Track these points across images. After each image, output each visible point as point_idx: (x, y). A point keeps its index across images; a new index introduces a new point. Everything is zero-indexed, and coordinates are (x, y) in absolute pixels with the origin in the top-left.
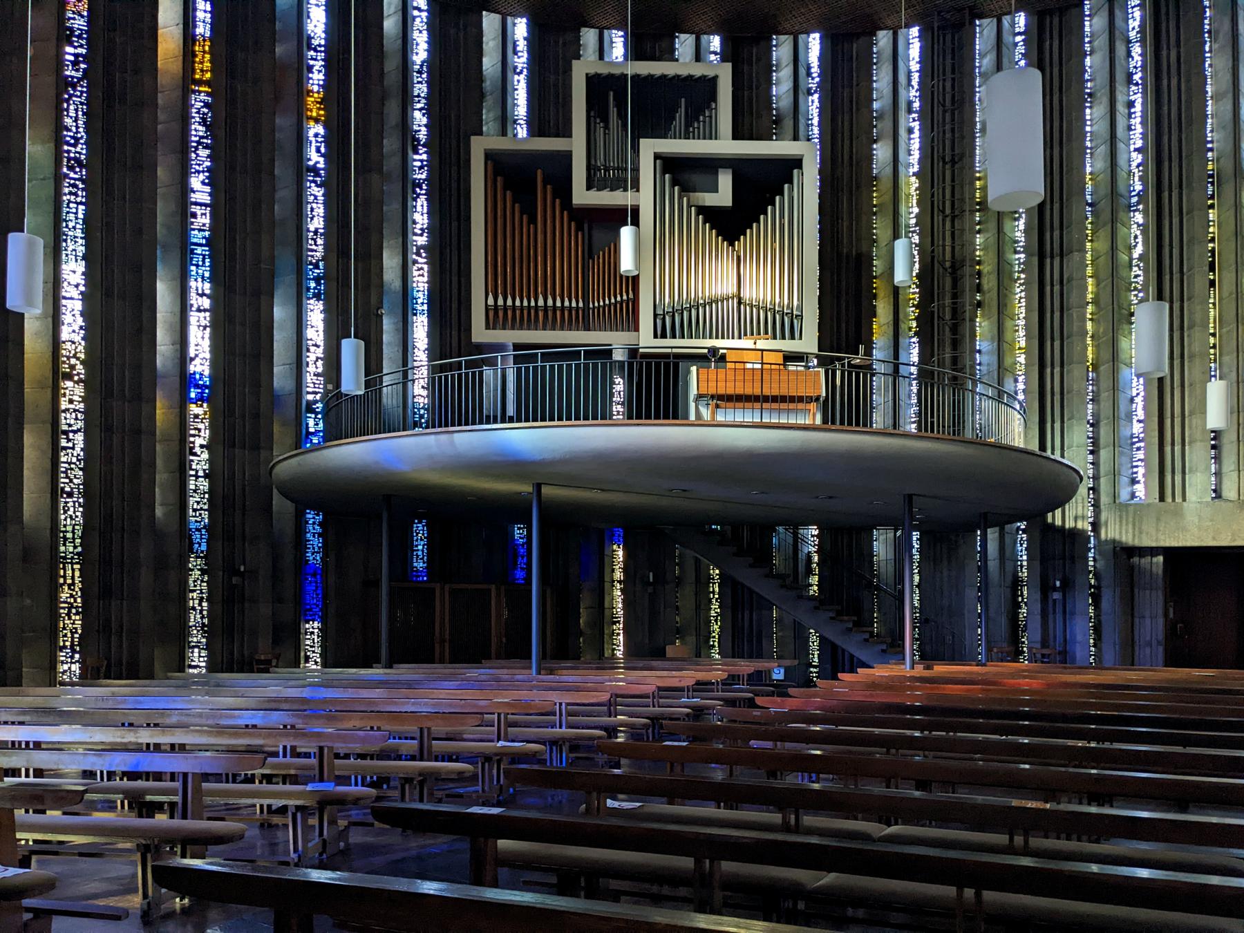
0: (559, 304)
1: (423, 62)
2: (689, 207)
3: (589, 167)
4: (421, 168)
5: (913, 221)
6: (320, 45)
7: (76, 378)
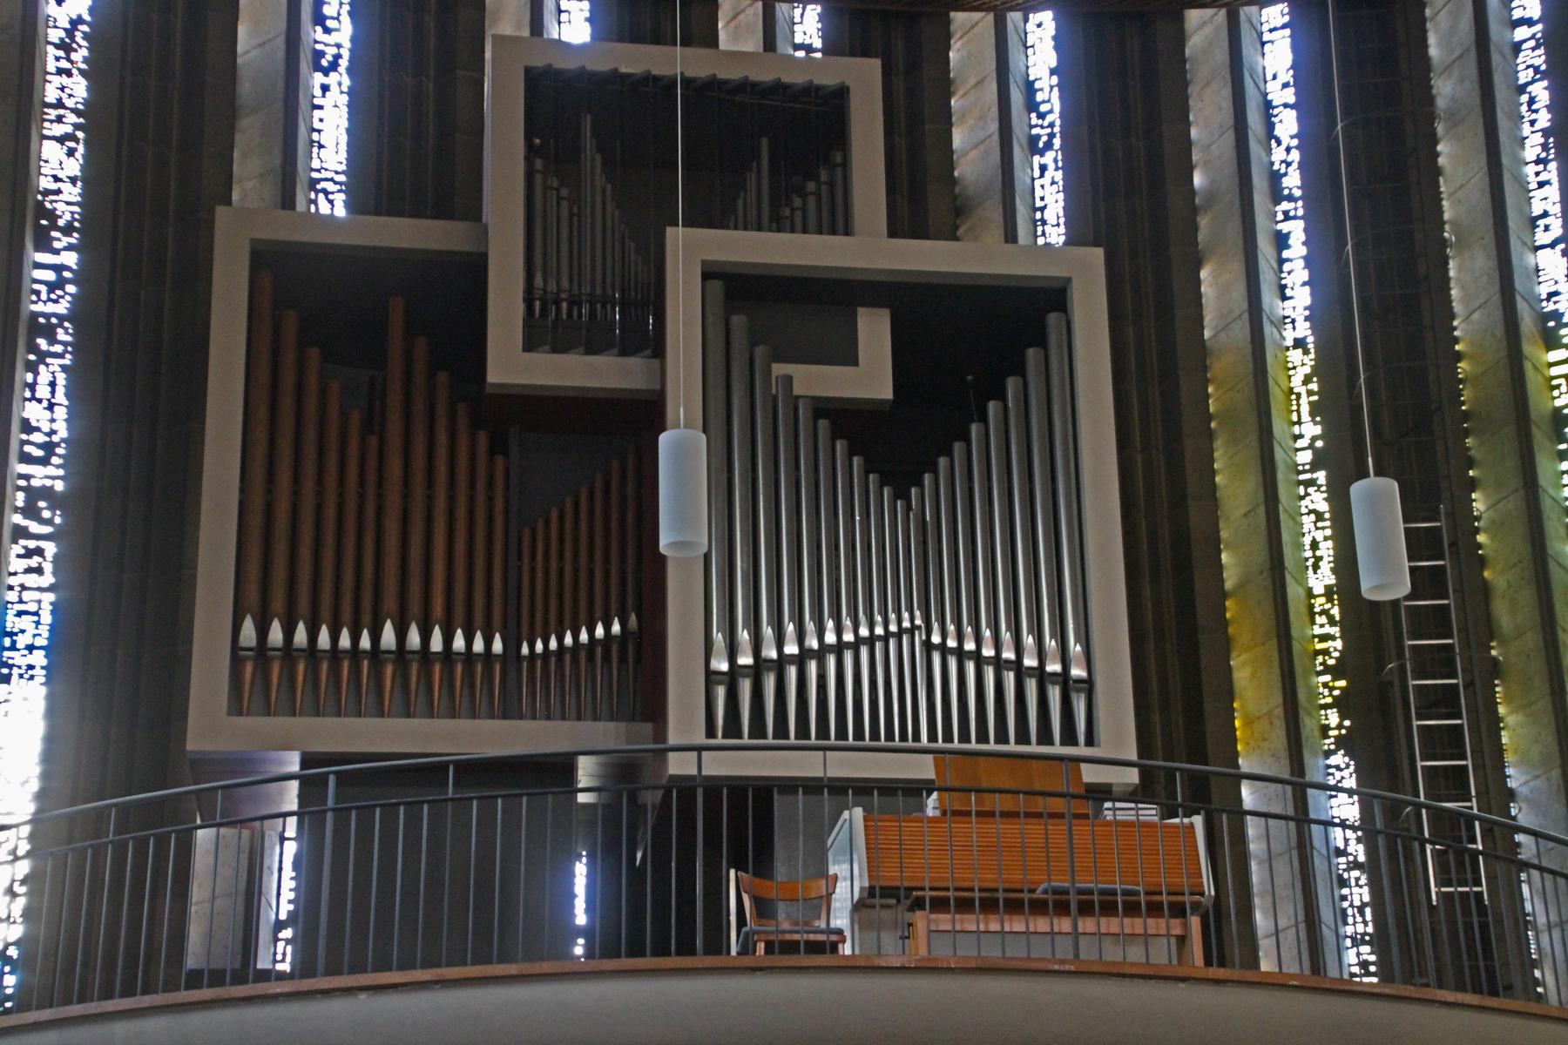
1: (76, 22)
4: (59, 284)
5: (1305, 457)
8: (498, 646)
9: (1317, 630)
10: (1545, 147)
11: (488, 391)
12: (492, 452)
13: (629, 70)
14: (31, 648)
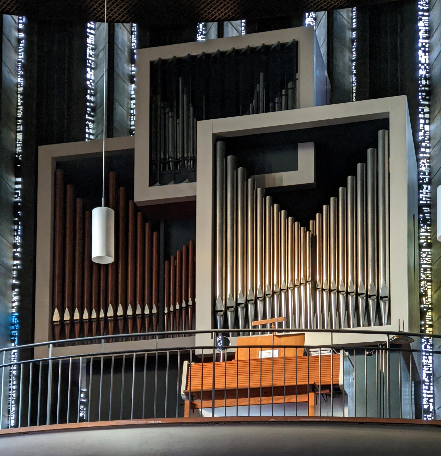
0: (147, 312)
3: (152, 163)
8: (155, 311)
12: (152, 230)
13: (196, 54)
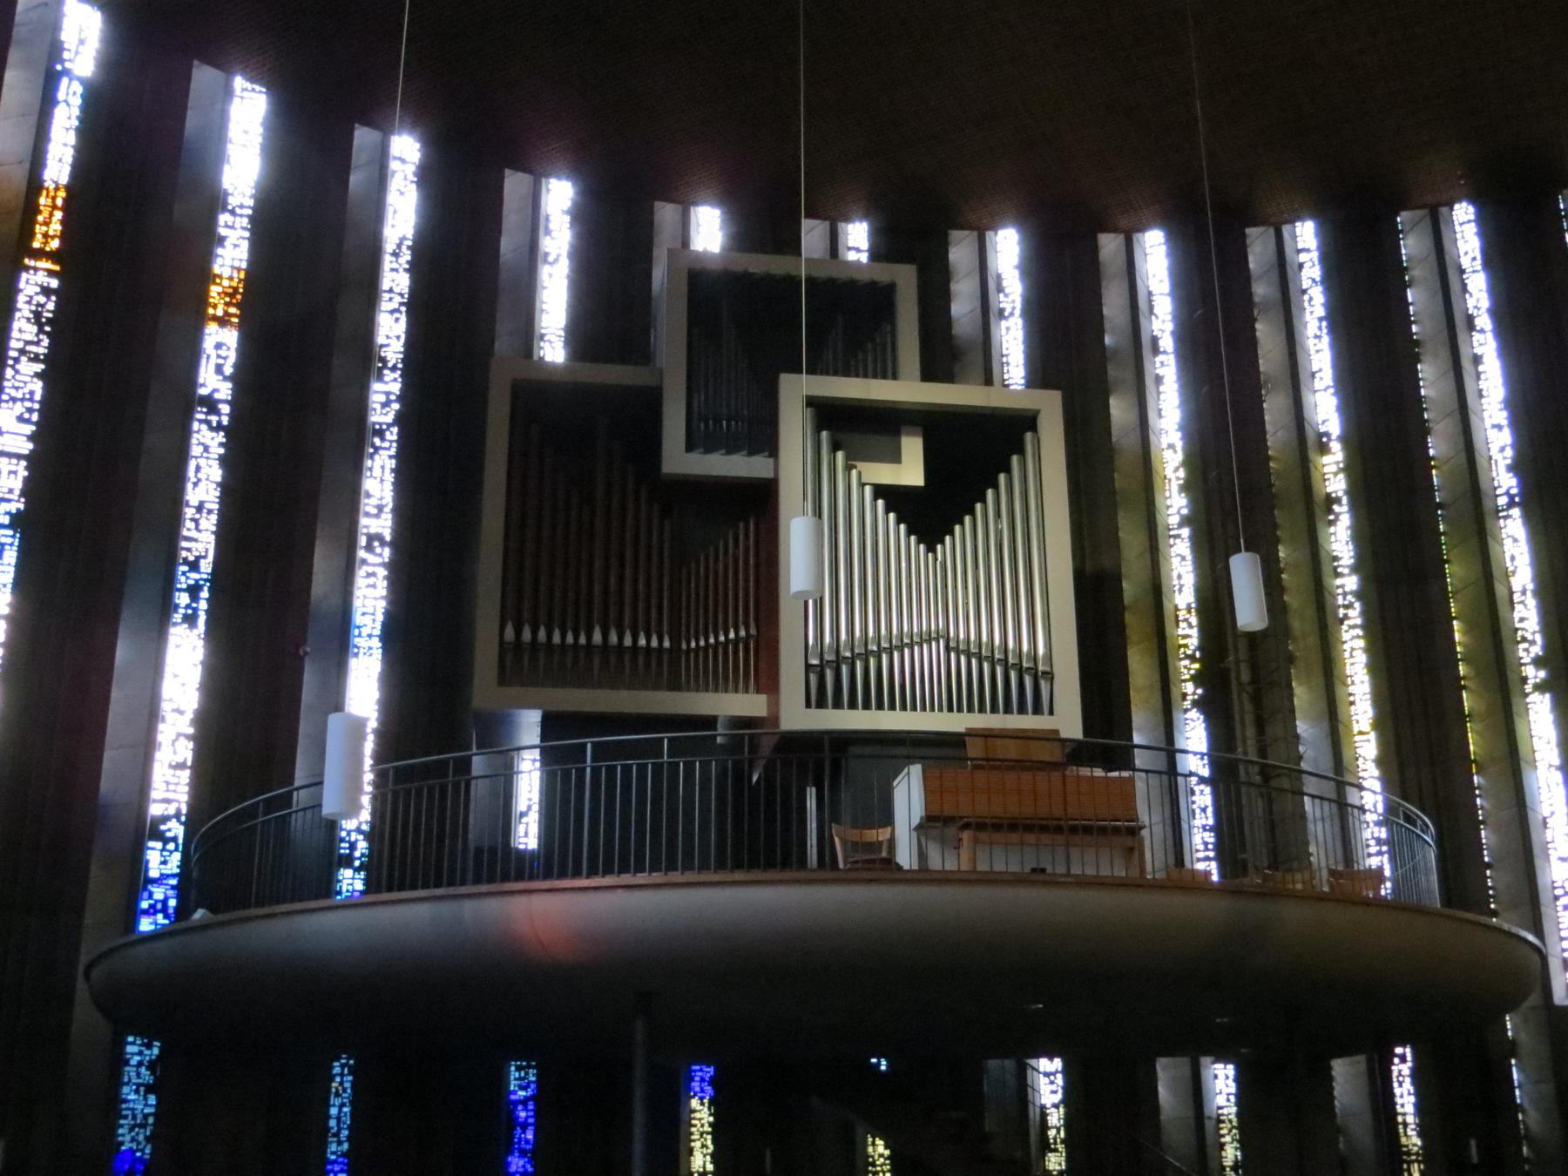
2: (862, 485)
6: (241, 207)
7: (357, 863)
8: (667, 644)
9: (1180, 632)
10: (1320, 328)
11: (203, 76)
14: (370, 636)
